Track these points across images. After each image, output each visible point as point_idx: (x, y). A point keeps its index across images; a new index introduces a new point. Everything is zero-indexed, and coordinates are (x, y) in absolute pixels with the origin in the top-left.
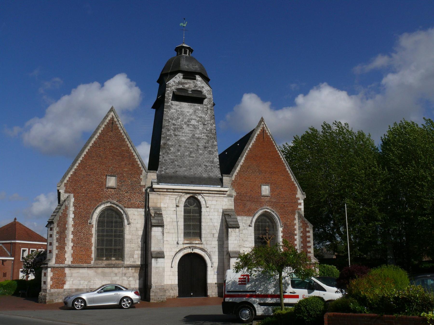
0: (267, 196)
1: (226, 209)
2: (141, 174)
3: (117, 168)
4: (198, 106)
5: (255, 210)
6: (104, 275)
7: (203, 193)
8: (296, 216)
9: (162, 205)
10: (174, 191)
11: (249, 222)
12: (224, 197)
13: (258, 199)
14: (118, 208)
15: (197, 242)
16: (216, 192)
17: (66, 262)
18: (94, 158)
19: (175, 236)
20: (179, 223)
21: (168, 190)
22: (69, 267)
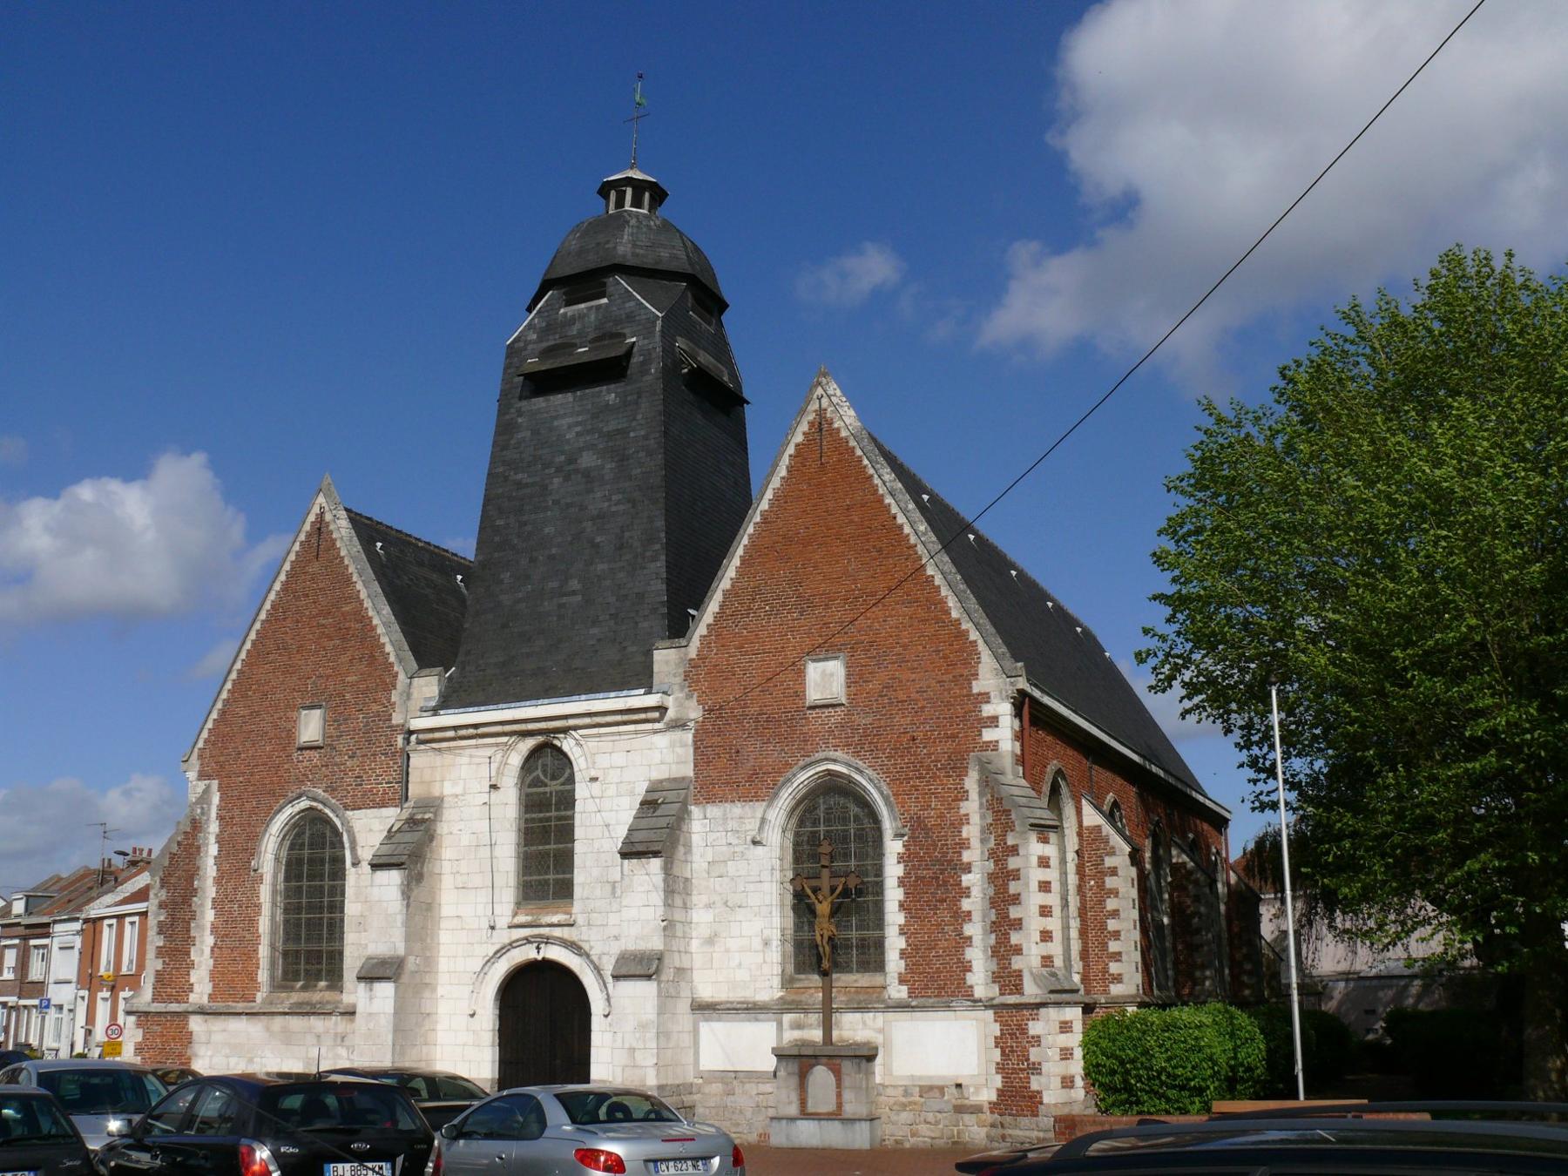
0: (833, 706)
1: (661, 781)
2: (394, 687)
3: (328, 677)
4: (609, 394)
5: (780, 773)
6: (288, 1039)
7: (576, 728)
8: (971, 782)
9: (448, 789)
10: (477, 732)
11: (751, 826)
12: (656, 732)
13: (790, 723)
14: (327, 811)
15: (555, 919)
16: (619, 718)
17: (193, 998)
18: (271, 657)
19: (484, 896)
20: (498, 852)
21: (481, 730)
22: (202, 1012)
